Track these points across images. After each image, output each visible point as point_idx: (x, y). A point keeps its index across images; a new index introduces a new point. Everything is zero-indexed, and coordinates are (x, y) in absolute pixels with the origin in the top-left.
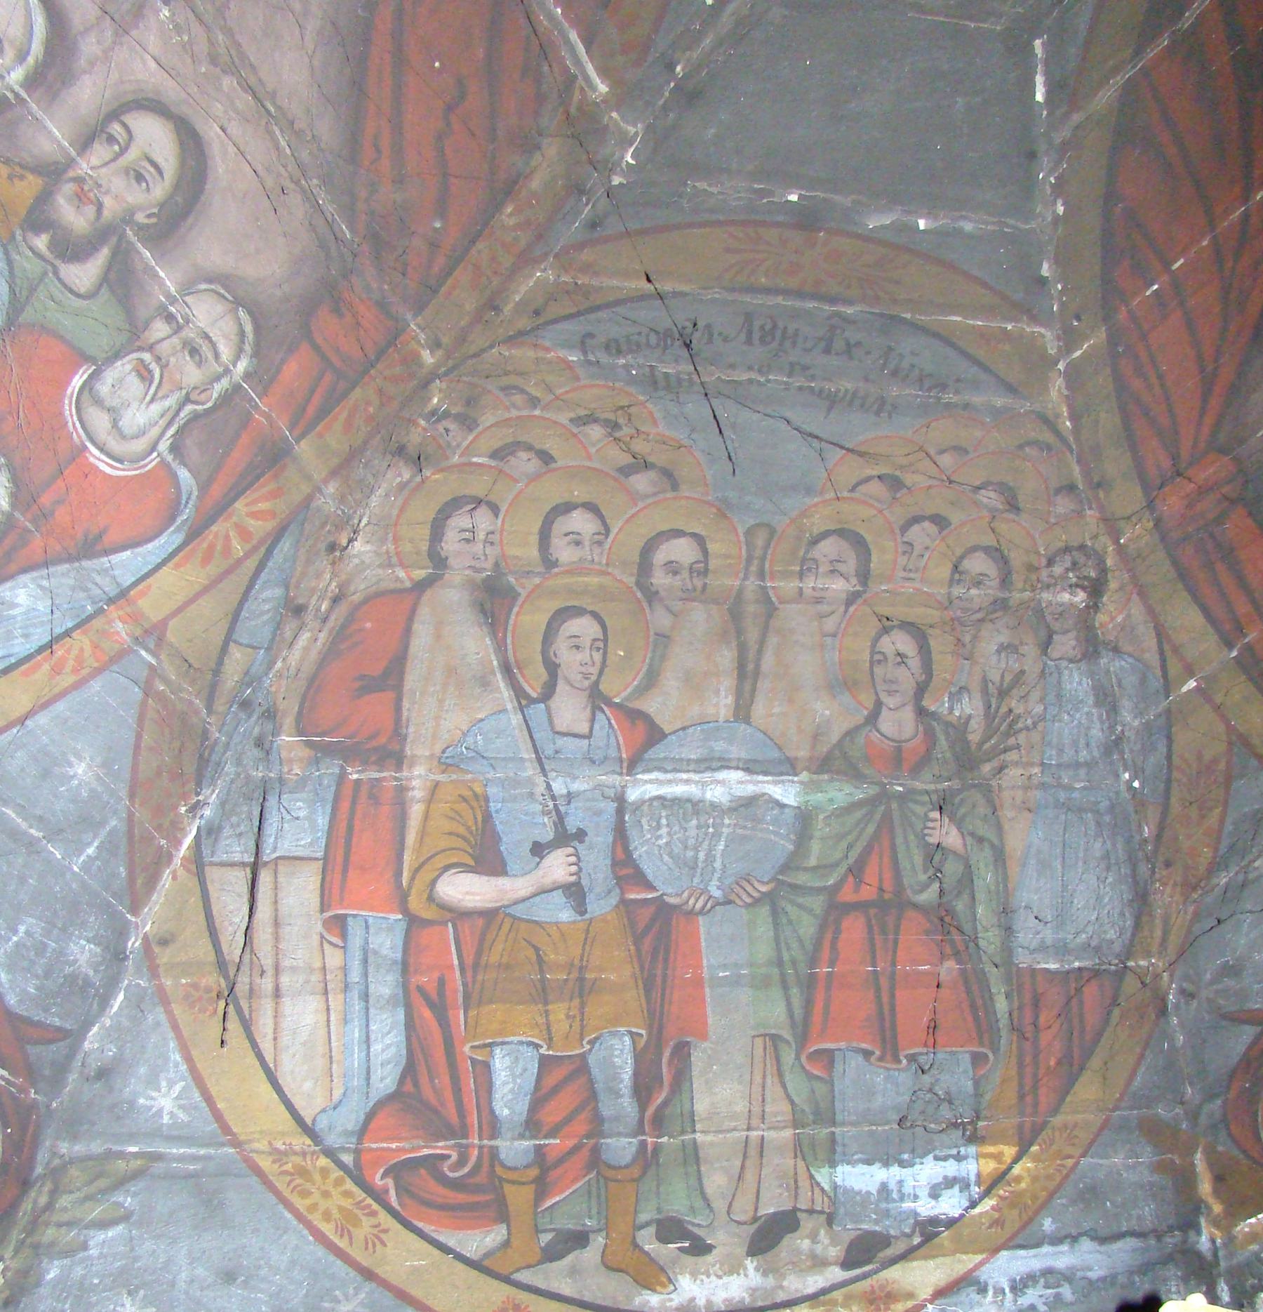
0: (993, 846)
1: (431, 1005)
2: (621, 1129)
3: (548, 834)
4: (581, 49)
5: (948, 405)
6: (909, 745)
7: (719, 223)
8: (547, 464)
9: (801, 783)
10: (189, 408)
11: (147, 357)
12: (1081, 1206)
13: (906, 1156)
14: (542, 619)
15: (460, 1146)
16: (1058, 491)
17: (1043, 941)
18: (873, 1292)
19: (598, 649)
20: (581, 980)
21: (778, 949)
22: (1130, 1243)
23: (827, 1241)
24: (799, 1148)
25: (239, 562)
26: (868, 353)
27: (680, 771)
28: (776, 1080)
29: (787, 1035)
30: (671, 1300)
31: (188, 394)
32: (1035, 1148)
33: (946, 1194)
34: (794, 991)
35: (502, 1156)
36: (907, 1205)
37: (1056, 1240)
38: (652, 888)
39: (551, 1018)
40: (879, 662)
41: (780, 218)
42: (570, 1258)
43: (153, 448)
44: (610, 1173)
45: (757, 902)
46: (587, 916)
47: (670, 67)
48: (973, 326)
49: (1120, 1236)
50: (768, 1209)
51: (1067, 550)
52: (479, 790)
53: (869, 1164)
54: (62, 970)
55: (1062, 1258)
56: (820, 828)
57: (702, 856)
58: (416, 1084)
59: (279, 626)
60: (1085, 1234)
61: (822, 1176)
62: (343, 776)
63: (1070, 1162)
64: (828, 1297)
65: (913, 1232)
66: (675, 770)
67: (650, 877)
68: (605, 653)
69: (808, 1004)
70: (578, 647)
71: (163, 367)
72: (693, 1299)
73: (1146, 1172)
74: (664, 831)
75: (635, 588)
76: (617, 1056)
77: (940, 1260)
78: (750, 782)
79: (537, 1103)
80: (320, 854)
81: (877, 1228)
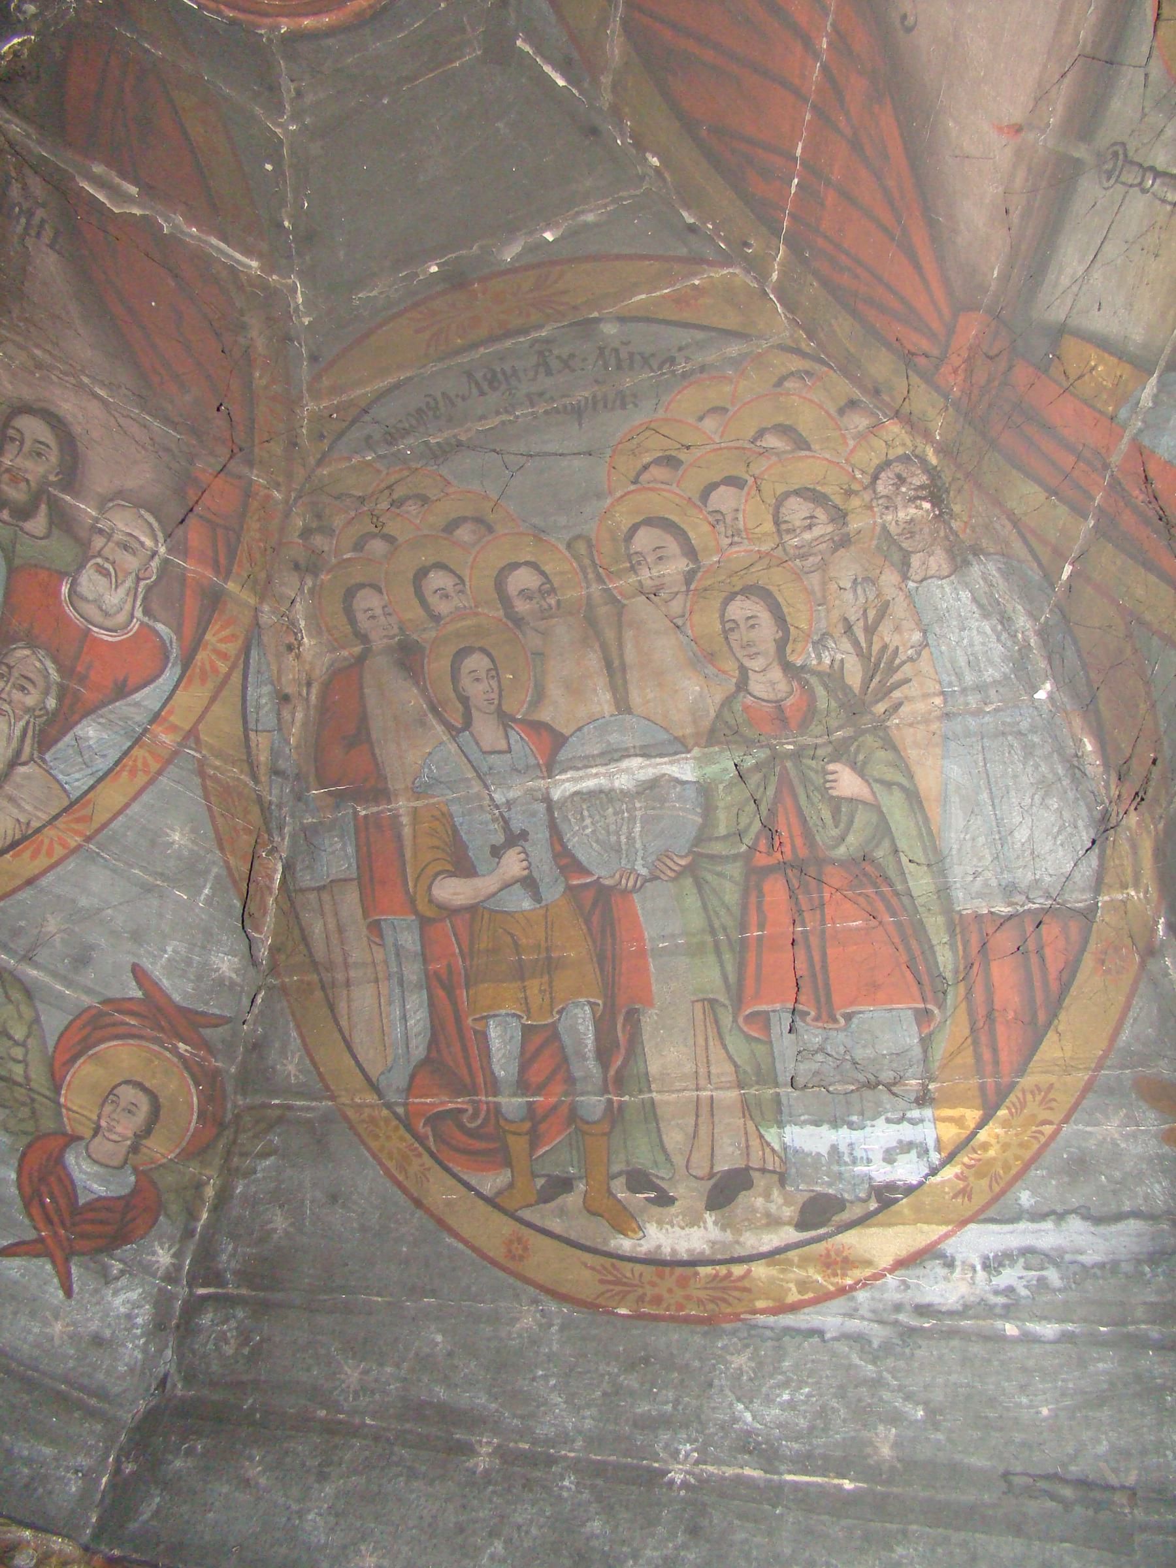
0: (902, 788)
1: (444, 987)
2: (590, 1088)
3: (500, 838)
4: (223, 245)
5: (684, 375)
6: (788, 702)
7: (401, 314)
8: (392, 543)
9: (694, 758)
10: (142, 584)
11: (99, 560)
12: (1066, 1179)
13: (855, 1118)
14: (446, 663)
15: (473, 1102)
16: (841, 411)
17: (986, 884)
18: (828, 1255)
19: (493, 677)
20: (549, 958)
21: (709, 918)
22: (1133, 1225)
23: (780, 1201)
24: (747, 1108)
25: (228, 676)
26: (584, 360)
27: (592, 767)
28: (718, 1043)
29: (723, 998)
30: (641, 1246)
31: (137, 575)
32: (1002, 1113)
33: (902, 1159)
34: (727, 956)
35: (504, 1110)
36: (860, 1169)
37: (1037, 1216)
38: (588, 873)
39: (528, 992)
40: (732, 630)
41: (438, 288)
42: (559, 1200)
43: (132, 616)
44: (585, 1127)
45: (679, 875)
46: (544, 903)
47: (280, 226)
48: (663, 297)
49: (1119, 1217)
50: (722, 1167)
51: (887, 464)
52: (444, 809)
53: (817, 1126)
54: (209, 976)
55: (1047, 1236)
56: (724, 799)
57: (623, 839)
58: (438, 1051)
59: (279, 714)
60: (1074, 1211)
61: (771, 1135)
62: (356, 813)
63: (1048, 1129)
64: (783, 1256)
65: (869, 1197)
66: (586, 767)
67: (585, 863)
68: (499, 682)
69: (741, 966)
70: (477, 680)
71: (113, 563)
72: (659, 1247)
73: (1153, 1142)
74: (588, 821)
75: (504, 620)
76: (581, 1024)
77: (899, 1228)
78: (650, 765)
79: (524, 1068)
80: (355, 876)
81: (830, 1191)
